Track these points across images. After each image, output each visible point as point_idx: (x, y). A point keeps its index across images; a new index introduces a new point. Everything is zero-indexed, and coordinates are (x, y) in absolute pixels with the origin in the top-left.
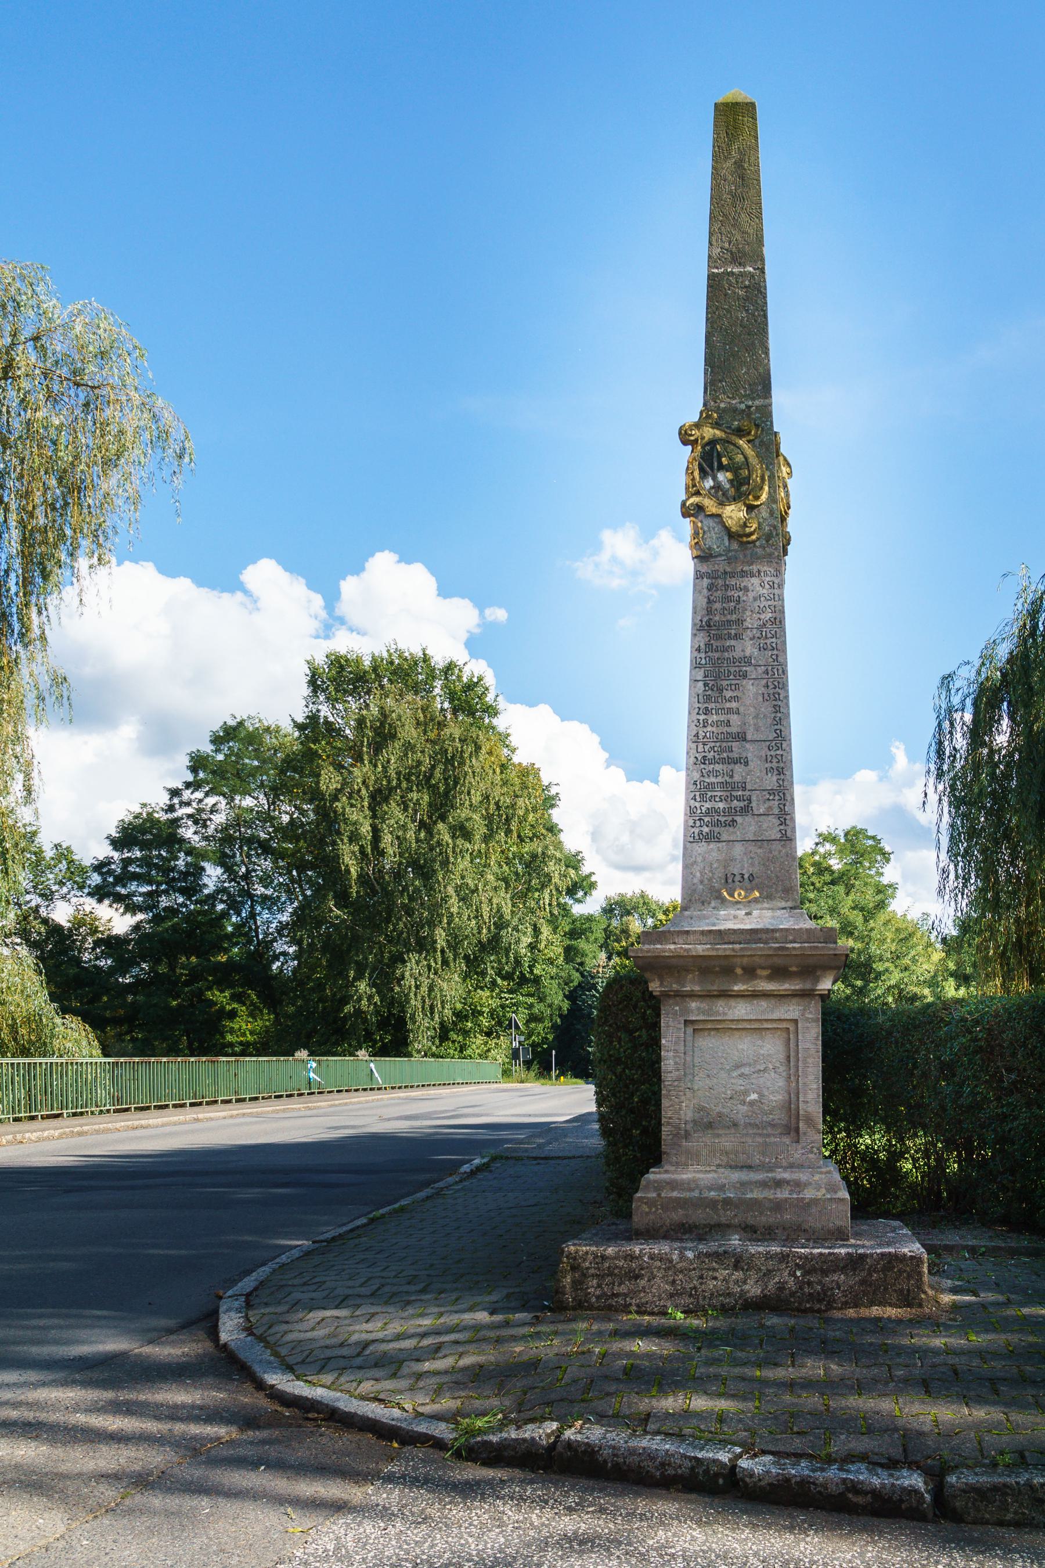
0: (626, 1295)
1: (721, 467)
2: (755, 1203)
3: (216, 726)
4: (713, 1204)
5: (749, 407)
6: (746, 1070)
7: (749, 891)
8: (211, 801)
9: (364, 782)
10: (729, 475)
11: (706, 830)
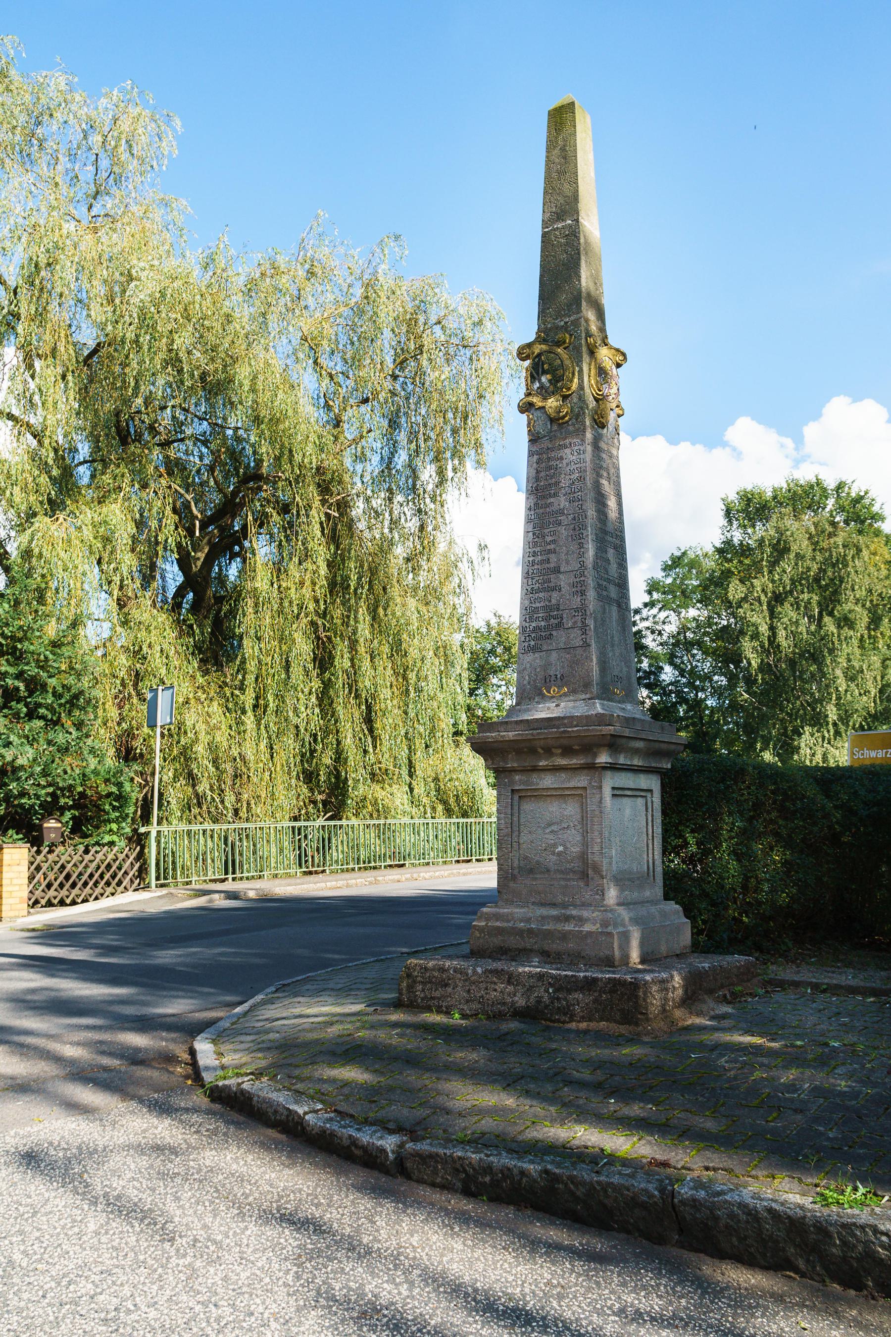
0: (439, 999)
1: (545, 372)
2: (548, 934)
3: (667, 558)
4: (520, 933)
5: (566, 323)
6: (554, 828)
7: (560, 687)
8: (662, 615)
9: (763, 590)
10: (549, 377)
11: (532, 643)
